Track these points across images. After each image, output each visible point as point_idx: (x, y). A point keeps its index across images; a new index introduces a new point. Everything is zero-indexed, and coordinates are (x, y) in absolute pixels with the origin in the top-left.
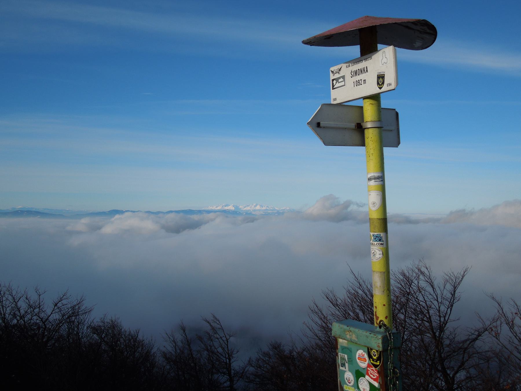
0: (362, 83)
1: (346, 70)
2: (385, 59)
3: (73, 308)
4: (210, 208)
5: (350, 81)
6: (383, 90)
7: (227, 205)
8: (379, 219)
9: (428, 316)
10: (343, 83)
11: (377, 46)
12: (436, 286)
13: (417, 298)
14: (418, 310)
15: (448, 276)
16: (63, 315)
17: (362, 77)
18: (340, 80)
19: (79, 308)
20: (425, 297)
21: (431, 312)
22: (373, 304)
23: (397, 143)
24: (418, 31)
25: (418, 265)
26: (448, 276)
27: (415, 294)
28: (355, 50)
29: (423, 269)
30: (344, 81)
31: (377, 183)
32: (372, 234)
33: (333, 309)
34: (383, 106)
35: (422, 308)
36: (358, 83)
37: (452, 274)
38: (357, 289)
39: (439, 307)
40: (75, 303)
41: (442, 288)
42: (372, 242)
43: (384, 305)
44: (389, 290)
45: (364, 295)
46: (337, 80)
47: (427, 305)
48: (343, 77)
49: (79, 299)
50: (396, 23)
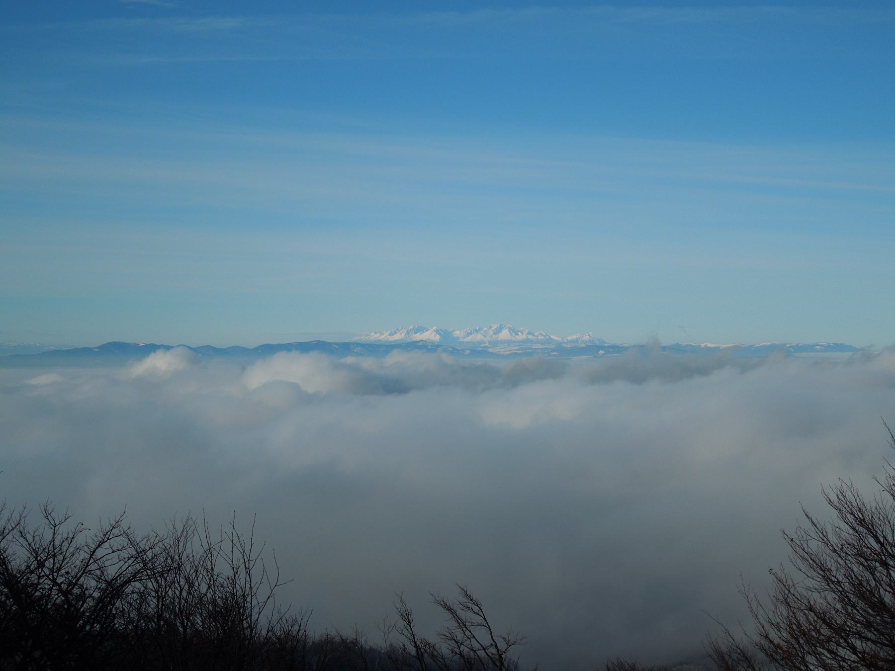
4: (384, 337)
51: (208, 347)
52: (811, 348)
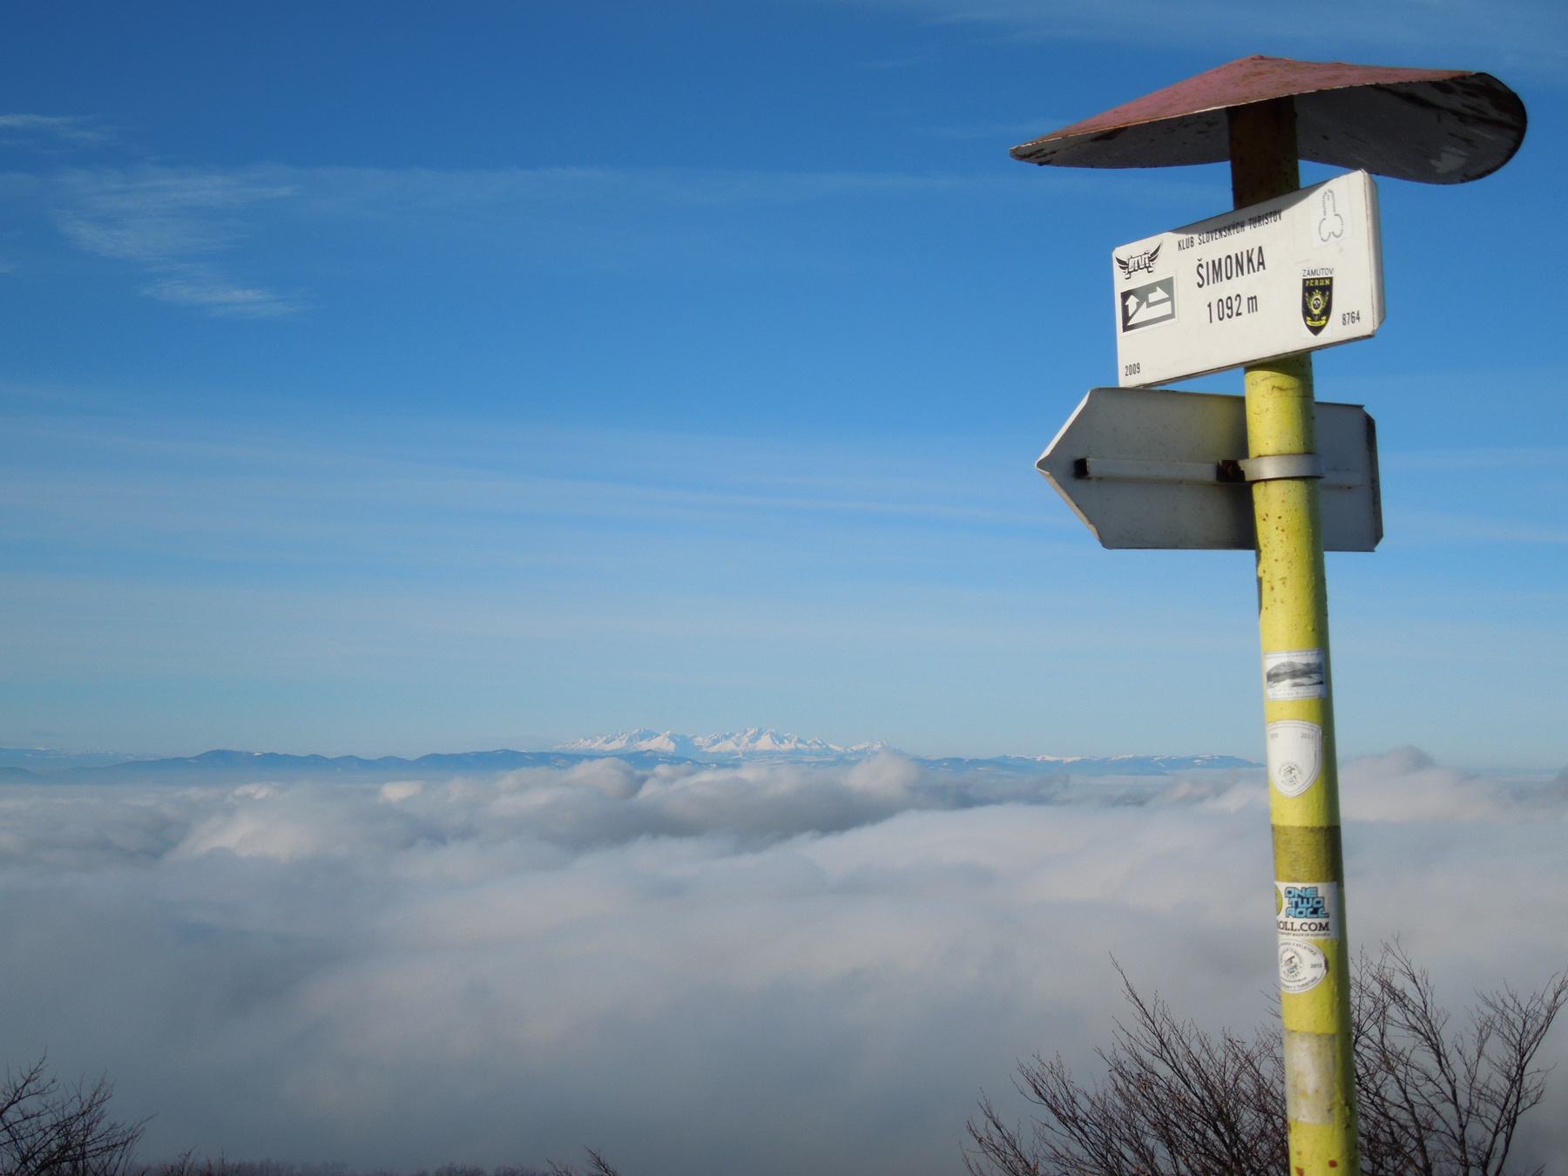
0: (1244, 309)
1: (1177, 256)
2: (1333, 221)
3: (63, 1127)
4: (583, 745)
5: (1193, 299)
6: (1325, 337)
7: (649, 735)
8: (1312, 830)
9: (1420, 1163)
10: (1165, 309)
11: (1296, 169)
12: (1447, 1046)
13: (1377, 1094)
14: (1382, 1137)
15: (1495, 1007)
16: (24, 1160)
17: (1242, 285)
18: (1152, 297)
19: (88, 1129)
20: (1409, 1089)
21: (1431, 1144)
22: (1286, 1154)
23: (1368, 535)
24: (1455, 113)
25: (1382, 967)
26: (1495, 1007)
27: (1372, 1076)
28: (1213, 182)
29: (1400, 982)
30: (1171, 298)
31: (1301, 690)
32: (1282, 886)
33: (1060, 1137)
34: (1322, 394)
35: (1396, 1129)
36: (1227, 309)
37: (1510, 1003)
38: (1147, 1057)
39: (1463, 1127)
40: (73, 1109)
41: (1472, 1052)
42: (1282, 917)
43: (1333, 1164)
44: (1349, 1103)
45: (1177, 1082)
46: (1142, 294)
47: (1416, 1120)
48: (1167, 285)
49: (87, 1095)
50: (1377, 87)
51: (314, 756)
52: (1187, 763)
